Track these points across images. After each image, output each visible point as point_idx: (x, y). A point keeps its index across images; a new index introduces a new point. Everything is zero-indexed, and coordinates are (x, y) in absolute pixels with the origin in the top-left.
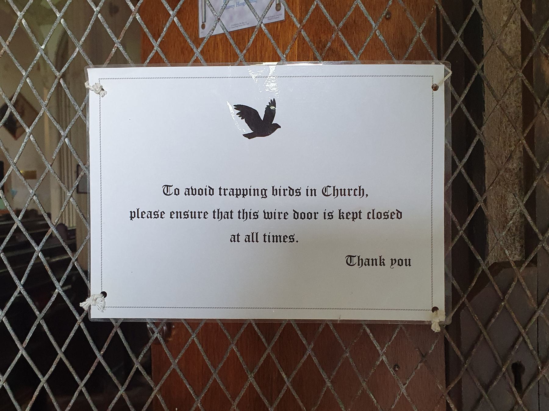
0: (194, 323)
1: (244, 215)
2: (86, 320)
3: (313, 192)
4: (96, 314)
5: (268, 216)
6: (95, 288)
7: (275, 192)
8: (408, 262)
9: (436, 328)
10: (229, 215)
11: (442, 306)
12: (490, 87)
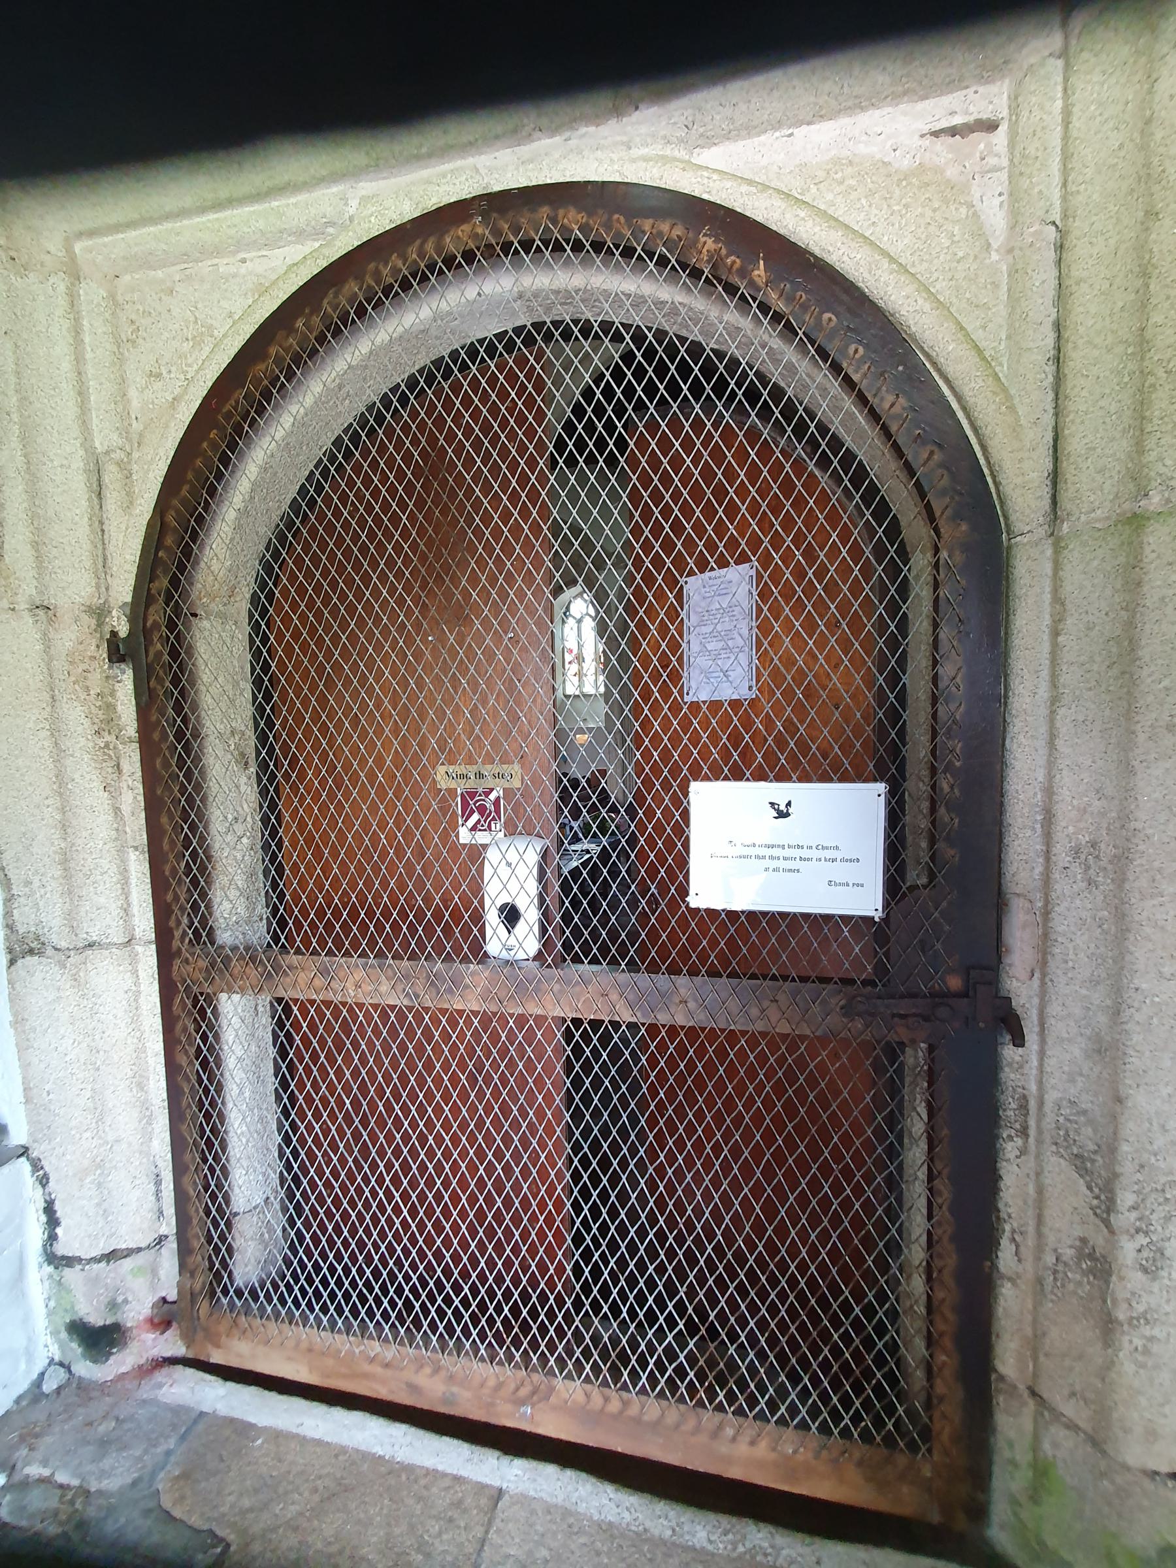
0: (846, 919)
1: (772, 858)
2: (687, 907)
3: (811, 847)
4: (693, 905)
5: (785, 859)
6: (692, 892)
7: (789, 847)
8: (862, 886)
9: (877, 919)
10: (764, 857)
11: (880, 909)
12: (103, 565)
